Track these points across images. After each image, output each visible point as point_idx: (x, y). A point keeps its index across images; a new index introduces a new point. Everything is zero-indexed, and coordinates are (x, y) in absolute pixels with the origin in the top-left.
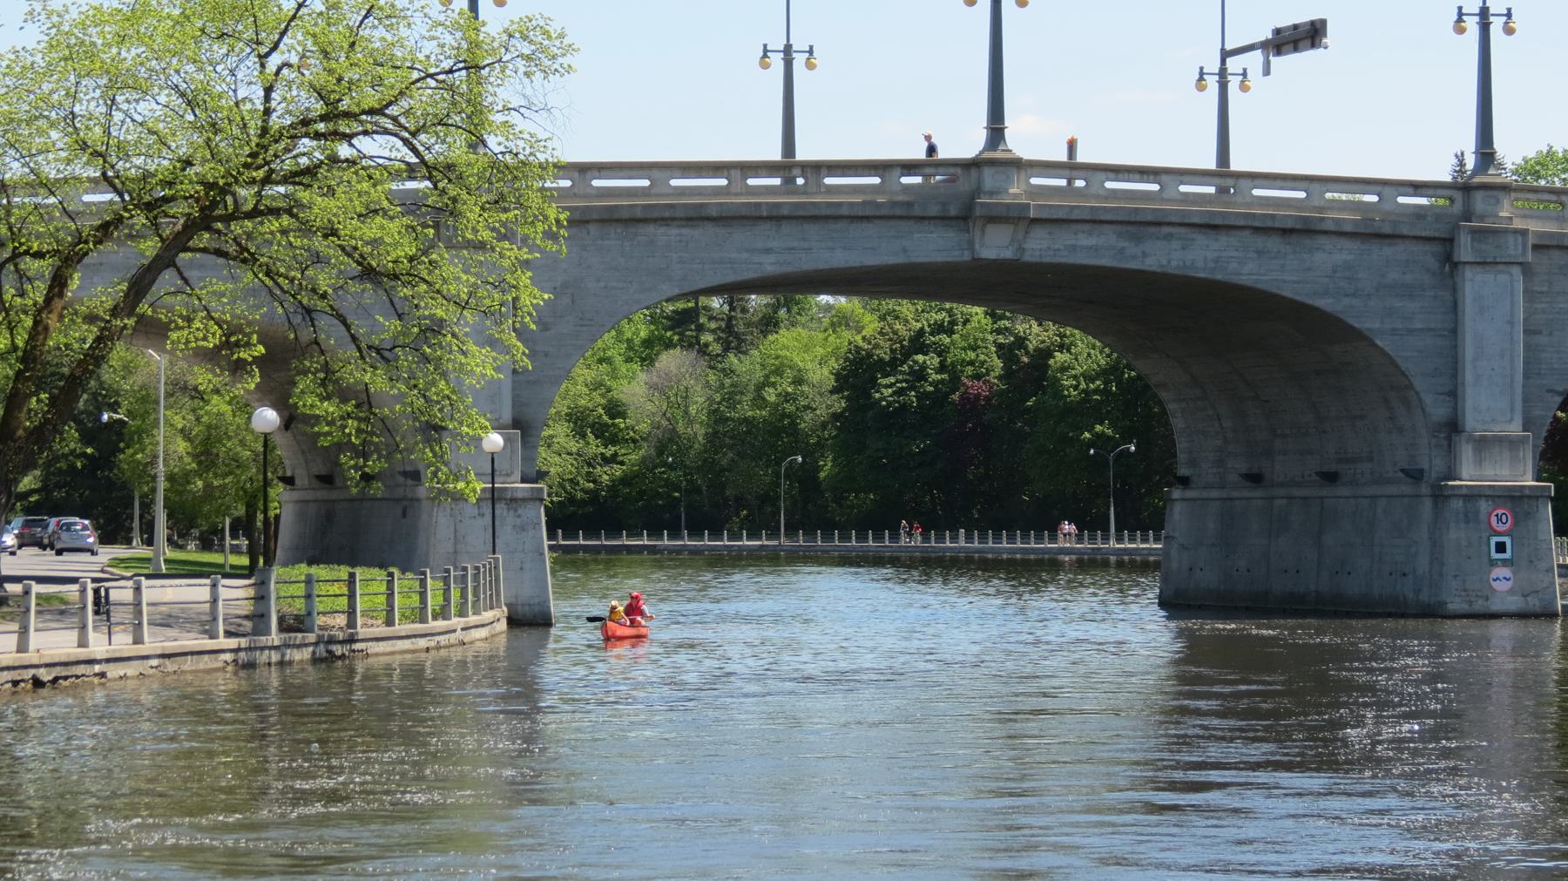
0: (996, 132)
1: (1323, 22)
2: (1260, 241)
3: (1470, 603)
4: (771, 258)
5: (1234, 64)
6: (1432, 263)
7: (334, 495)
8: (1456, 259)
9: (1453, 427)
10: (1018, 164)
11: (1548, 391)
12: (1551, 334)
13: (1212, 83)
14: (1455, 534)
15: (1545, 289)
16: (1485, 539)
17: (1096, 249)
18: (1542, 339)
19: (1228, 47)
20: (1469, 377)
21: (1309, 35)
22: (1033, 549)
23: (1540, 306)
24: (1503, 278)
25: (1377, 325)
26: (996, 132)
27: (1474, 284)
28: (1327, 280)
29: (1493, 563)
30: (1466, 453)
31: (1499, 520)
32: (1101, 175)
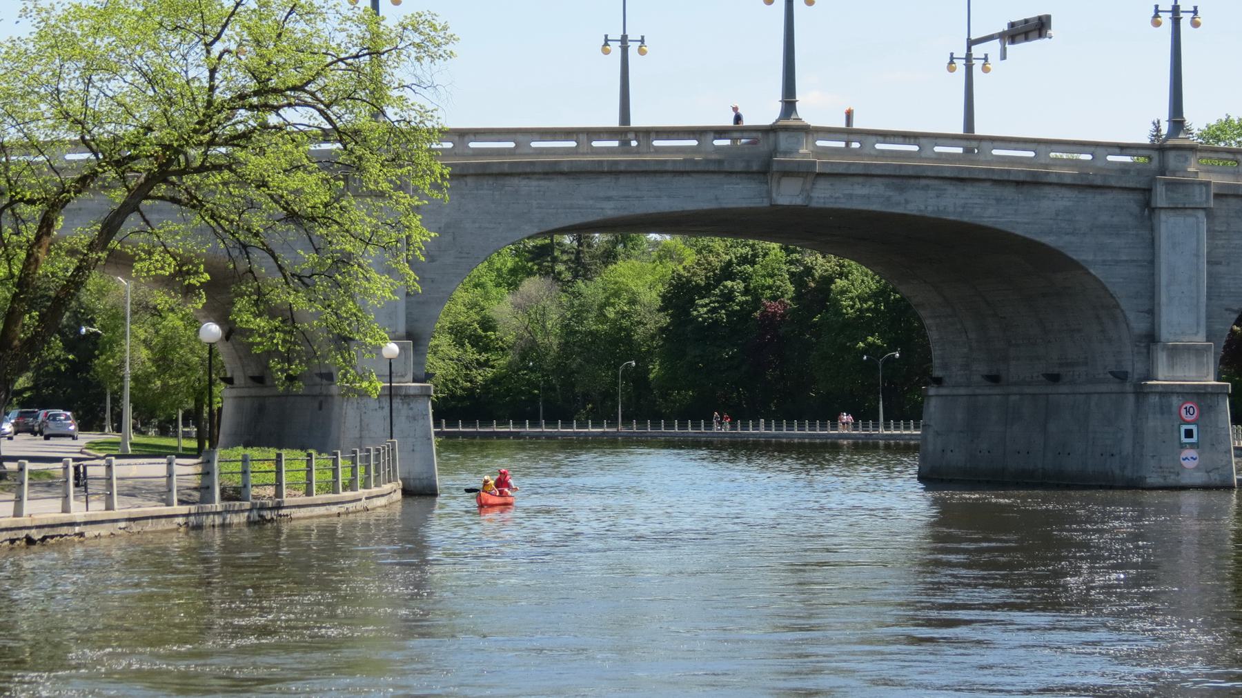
0: (789, 104)
1: (1048, 18)
2: (998, 191)
3: (1165, 478)
4: (611, 204)
5: (977, 51)
6: (1135, 208)
7: (265, 392)
8: (1153, 205)
9: (1151, 338)
10: (806, 130)
11: (1227, 310)
12: (1228, 264)
13: (960, 66)
14: (1153, 423)
15: (1224, 229)
16: (1176, 427)
17: (868, 197)
18: (1222, 269)
19: (973, 37)
20: (1164, 298)
21: (1037, 28)
22: (819, 435)
23: (1220, 242)
24: (1191, 220)
25: (1091, 258)
26: (789, 104)
27: (1168, 225)
28: (1051, 222)
29: (1183, 446)
30: (1162, 359)
31: (1188, 412)
32: (873, 139)
